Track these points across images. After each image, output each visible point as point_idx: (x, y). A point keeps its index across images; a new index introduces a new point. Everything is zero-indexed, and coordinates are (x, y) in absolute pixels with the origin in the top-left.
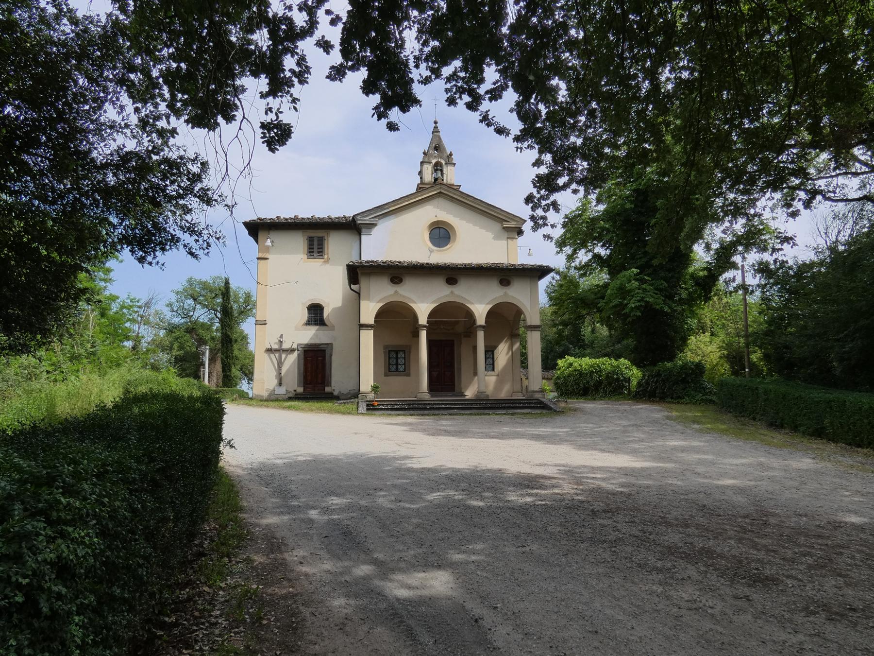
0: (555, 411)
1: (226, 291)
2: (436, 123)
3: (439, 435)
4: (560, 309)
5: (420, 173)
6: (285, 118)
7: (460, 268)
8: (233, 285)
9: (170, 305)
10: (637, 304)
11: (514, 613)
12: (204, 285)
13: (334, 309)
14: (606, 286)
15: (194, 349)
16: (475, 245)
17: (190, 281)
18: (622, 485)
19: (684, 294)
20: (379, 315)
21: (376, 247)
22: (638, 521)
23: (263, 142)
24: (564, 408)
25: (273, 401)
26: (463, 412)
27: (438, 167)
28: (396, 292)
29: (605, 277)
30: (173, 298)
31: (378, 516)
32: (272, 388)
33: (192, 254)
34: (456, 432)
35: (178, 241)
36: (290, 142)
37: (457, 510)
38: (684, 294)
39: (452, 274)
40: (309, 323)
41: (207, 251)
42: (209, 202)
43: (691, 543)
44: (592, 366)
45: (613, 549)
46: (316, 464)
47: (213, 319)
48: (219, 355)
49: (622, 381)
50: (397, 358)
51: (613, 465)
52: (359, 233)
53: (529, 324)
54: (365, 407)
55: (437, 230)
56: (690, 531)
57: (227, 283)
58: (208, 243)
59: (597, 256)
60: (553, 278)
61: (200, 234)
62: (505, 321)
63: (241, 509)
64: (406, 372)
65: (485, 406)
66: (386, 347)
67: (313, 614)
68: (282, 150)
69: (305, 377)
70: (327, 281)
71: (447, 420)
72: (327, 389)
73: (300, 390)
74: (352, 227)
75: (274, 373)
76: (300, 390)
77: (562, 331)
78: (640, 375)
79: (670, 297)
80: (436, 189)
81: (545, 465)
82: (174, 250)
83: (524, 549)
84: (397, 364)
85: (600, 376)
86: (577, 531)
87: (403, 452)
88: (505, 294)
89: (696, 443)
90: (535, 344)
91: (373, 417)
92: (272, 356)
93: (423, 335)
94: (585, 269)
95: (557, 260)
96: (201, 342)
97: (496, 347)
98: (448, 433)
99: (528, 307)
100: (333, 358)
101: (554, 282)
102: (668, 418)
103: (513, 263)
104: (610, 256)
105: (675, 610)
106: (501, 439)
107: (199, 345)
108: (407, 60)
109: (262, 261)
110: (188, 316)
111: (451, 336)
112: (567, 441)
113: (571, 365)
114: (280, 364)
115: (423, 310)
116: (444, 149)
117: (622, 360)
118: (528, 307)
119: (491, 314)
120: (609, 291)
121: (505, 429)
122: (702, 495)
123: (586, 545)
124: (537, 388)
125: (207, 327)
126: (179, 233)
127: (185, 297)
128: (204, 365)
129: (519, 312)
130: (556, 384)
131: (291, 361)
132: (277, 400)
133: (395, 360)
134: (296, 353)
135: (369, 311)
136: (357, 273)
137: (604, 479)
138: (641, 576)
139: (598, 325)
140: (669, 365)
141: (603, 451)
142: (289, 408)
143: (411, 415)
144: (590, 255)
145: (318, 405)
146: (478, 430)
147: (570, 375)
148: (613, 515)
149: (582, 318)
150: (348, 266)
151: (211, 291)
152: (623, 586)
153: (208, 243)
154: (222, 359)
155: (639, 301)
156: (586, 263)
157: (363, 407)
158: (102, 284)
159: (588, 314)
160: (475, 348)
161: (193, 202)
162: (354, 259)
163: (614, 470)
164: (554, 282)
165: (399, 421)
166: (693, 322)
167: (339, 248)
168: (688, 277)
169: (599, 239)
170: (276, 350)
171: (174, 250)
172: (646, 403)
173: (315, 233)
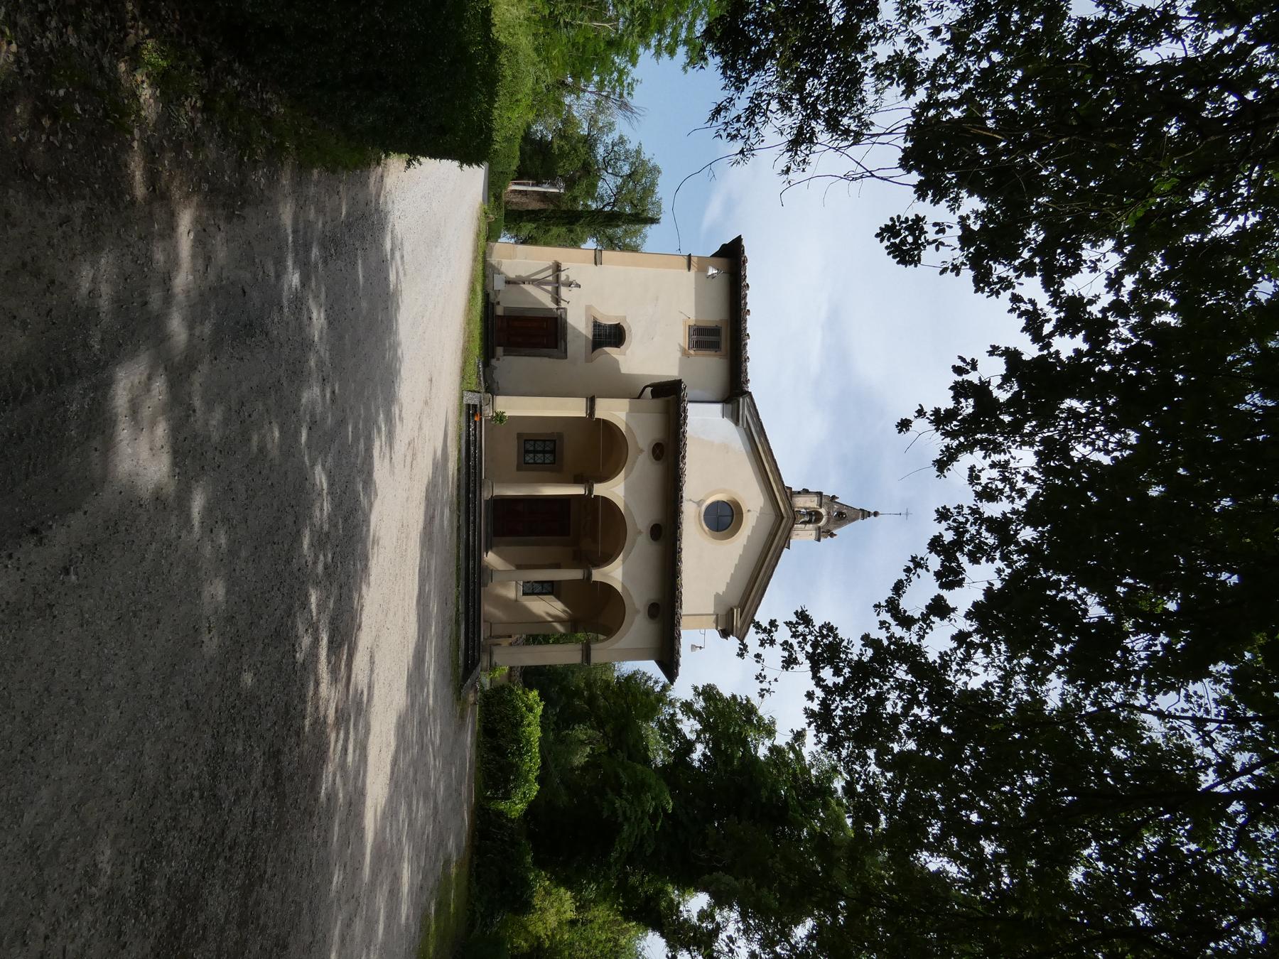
0: (462, 687)
1: (642, 218)
2: (876, 514)
3: (427, 507)
4: (613, 692)
5: (806, 491)
6: (928, 254)
7: (675, 544)
8: (649, 230)
9: (622, 141)
10: (620, 812)
11: (51, 606)
12: (649, 190)
13: (616, 361)
14: (647, 761)
15: (560, 172)
16: (708, 566)
17: (656, 170)
18: (331, 797)
19: (634, 880)
20: (608, 427)
21: (706, 423)
22: (255, 834)
23: (892, 219)
24: (466, 701)
25: (484, 269)
26: (462, 546)
27: (814, 516)
28: (642, 451)
29: (659, 759)
30: (632, 146)
31: (282, 378)
32: (503, 269)
33: (718, 111)
34: (431, 533)
35: (737, 89)
36: (892, 262)
37: (289, 520)
38: (634, 880)
39: (666, 534)
40: (597, 325)
41: (724, 135)
42: (794, 144)
43: (204, 938)
44: (528, 741)
45: (196, 794)
46: (382, 301)
47: (602, 198)
48: (552, 207)
49: (505, 787)
50: (544, 452)
51: (368, 781)
52: (724, 401)
53: (593, 646)
54: (472, 402)
55: (728, 512)
56: (232, 933)
57: (653, 221)
58: (736, 136)
59: (689, 747)
60: (656, 682)
61: (750, 125)
62: (596, 612)
63: (302, 168)
64: (522, 465)
65: (471, 581)
66: (560, 436)
67: (66, 220)
68: (881, 248)
69: (517, 318)
70: (655, 352)
71: (451, 521)
72: (500, 350)
73: (499, 311)
74: (734, 392)
75: (524, 273)
76: (499, 311)
77: (581, 696)
78: (514, 815)
79: (630, 859)
80: (788, 513)
81: (372, 671)
82: (724, 82)
83: (204, 630)
84: (535, 452)
85: (513, 754)
86: (239, 726)
87: (400, 446)
88: (638, 612)
89: (404, 909)
90: (562, 655)
91: (457, 413)
92: (550, 272)
93: (578, 490)
94: (671, 729)
95: (682, 690)
96: (571, 183)
97: (559, 598)
98: (429, 520)
99: (616, 646)
100: (546, 360)
101: (651, 683)
102: (447, 863)
103: (684, 621)
104: (689, 766)
105: (42, 929)
106: (418, 601)
107: (565, 181)
108: (1004, 451)
109: (685, 261)
110: (607, 164)
111: (579, 532)
112: (412, 705)
113: (531, 709)
114: (539, 283)
115: (614, 490)
116: (840, 526)
117: (536, 787)
118: (616, 646)
119: (607, 589)
120: (639, 767)
121: (434, 608)
122: (307, 938)
123: (209, 743)
124: (496, 659)
125: (590, 192)
126: (749, 91)
127: (633, 164)
128: (537, 185)
129: (610, 631)
130: (503, 687)
131: (543, 298)
132: (485, 276)
133: (541, 448)
134: (553, 306)
135: (614, 411)
136: (669, 395)
137: (343, 765)
138: (132, 851)
139: (588, 749)
140: (529, 859)
141: (395, 762)
142: (472, 290)
143: (459, 470)
144: (692, 737)
145: (477, 333)
146: (433, 568)
147: (515, 708)
148: (270, 789)
149: (600, 725)
150: (680, 382)
151: (642, 199)
152: (109, 818)
153: (736, 136)
154: (545, 210)
155: (624, 813)
156: (680, 731)
157: (472, 399)
158: (653, 42)
159: (605, 734)
160: (557, 566)
161: (790, 122)
162: (689, 392)
163: (360, 784)
164: (651, 683)
165: (450, 450)
166: (591, 891)
167: (710, 366)
168: (659, 885)
169: (715, 749)
170: (558, 277)
171: (724, 82)
172: (470, 825)
173: (724, 337)
